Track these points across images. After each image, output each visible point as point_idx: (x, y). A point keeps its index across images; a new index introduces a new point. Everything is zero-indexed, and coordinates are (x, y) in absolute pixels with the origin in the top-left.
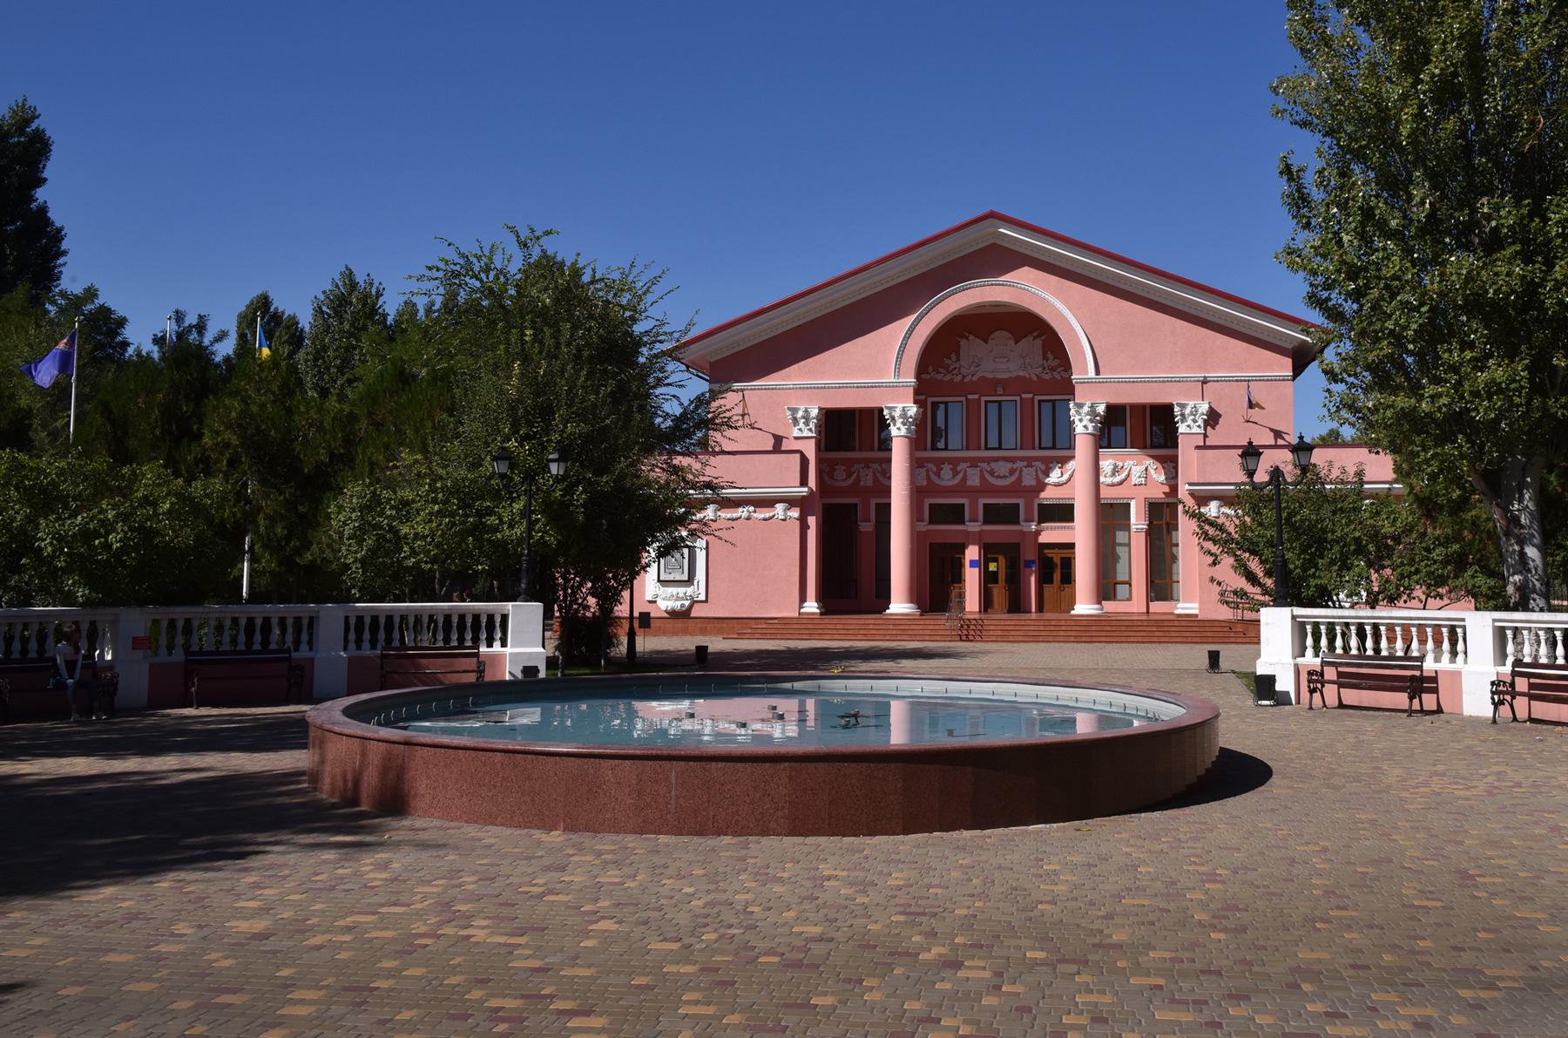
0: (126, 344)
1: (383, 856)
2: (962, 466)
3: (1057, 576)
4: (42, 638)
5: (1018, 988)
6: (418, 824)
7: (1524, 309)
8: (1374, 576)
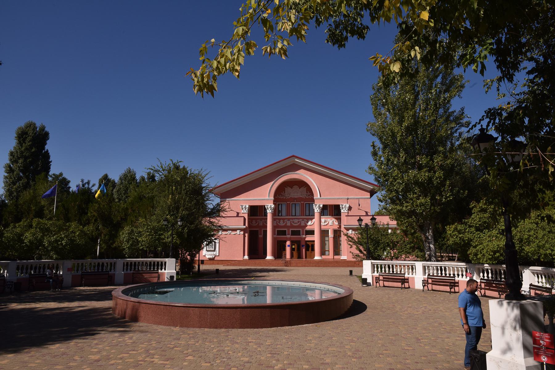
0: (70, 188)
2: (286, 220)
3: (310, 249)
4: (44, 269)
6: (141, 325)
7: (428, 184)
8: (392, 252)
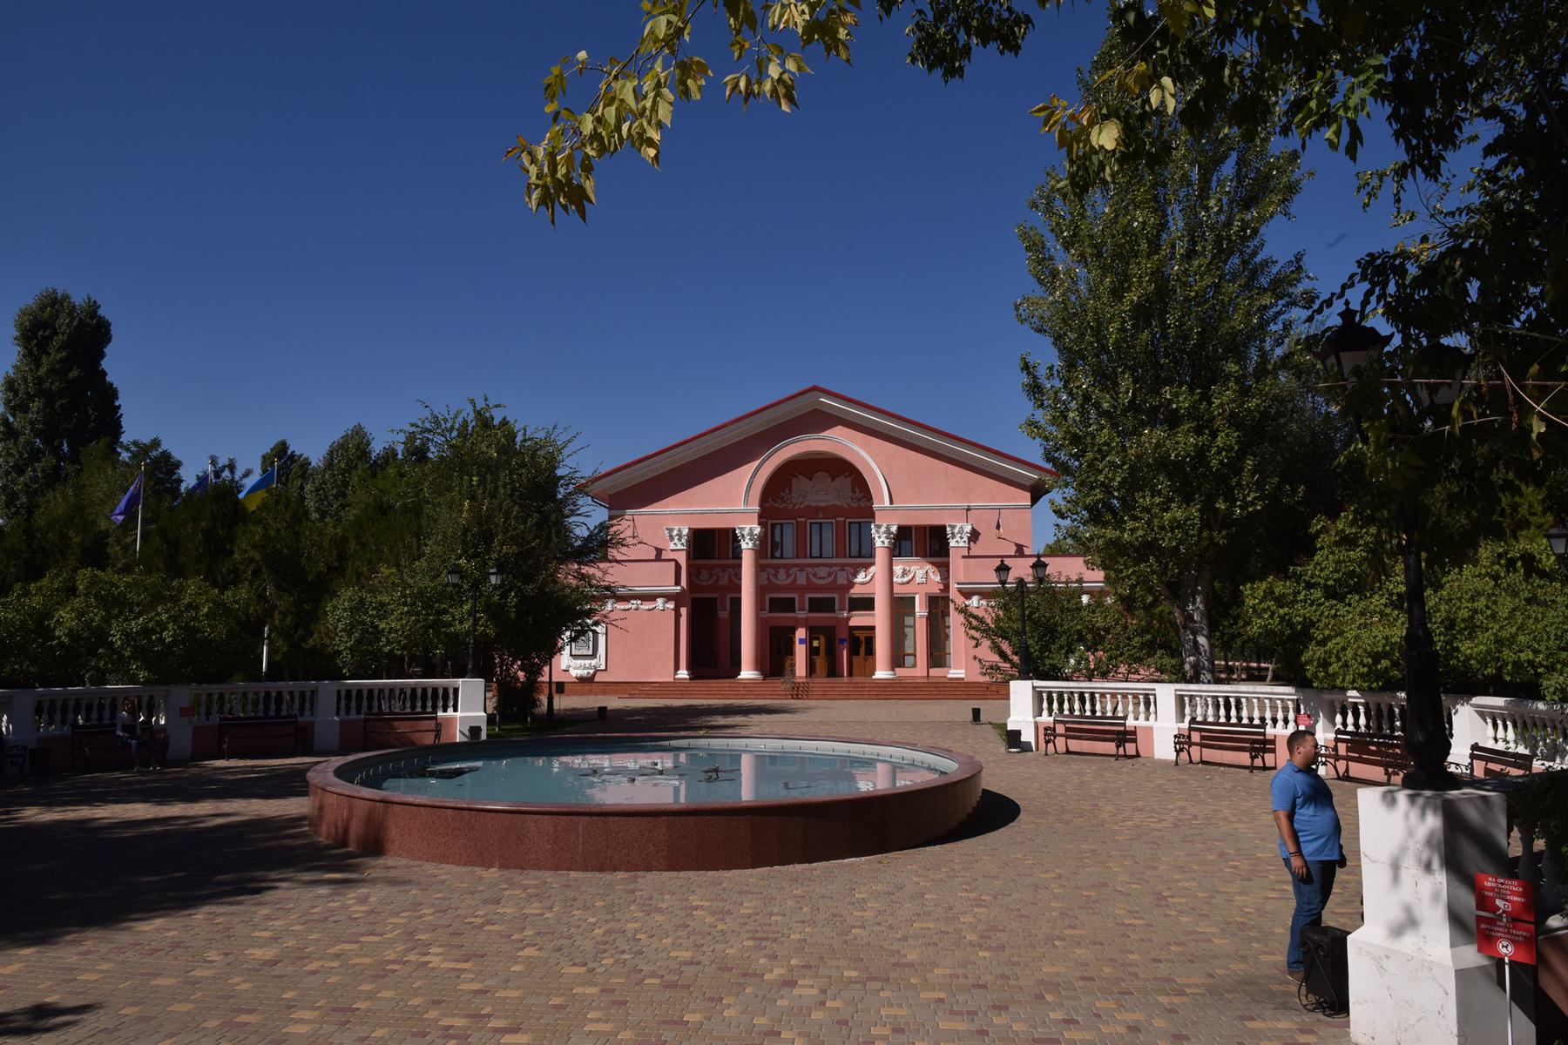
1: (363, 891)
3: (862, 650)
5: (838, 1004)
